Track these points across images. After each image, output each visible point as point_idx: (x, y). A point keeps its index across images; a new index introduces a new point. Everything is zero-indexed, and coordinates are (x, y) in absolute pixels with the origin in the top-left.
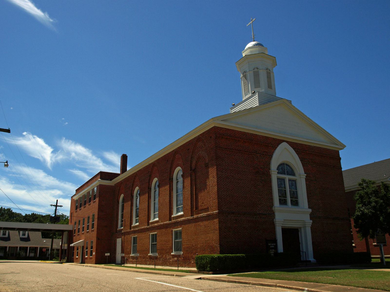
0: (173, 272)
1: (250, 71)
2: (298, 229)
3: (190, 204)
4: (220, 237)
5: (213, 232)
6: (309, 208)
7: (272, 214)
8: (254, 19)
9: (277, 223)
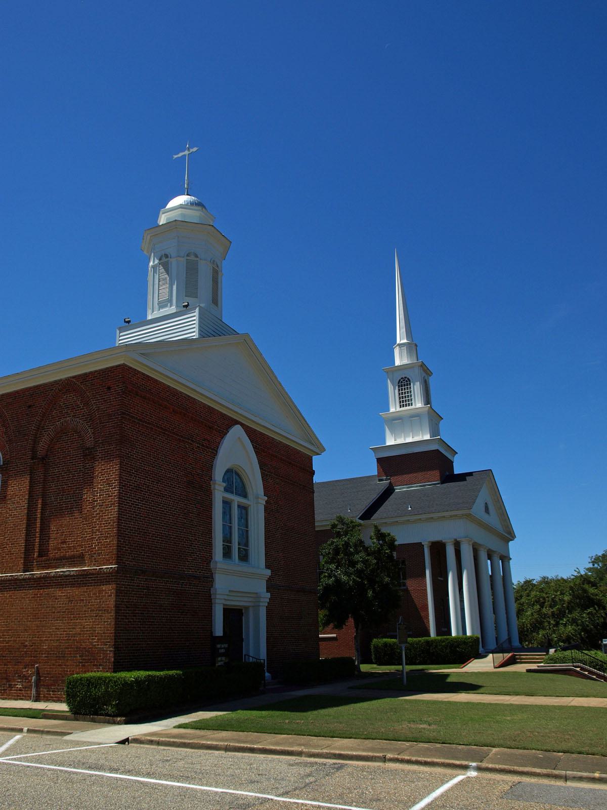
0: (21, 718)
1: (179, 256)
2: (242, 610)
3: (22, 542)
4: (115, 627)
5: (96, 616)
6: (267, 567)
7: (208, 579)
8: (195, 149)
9: (218, 596)
